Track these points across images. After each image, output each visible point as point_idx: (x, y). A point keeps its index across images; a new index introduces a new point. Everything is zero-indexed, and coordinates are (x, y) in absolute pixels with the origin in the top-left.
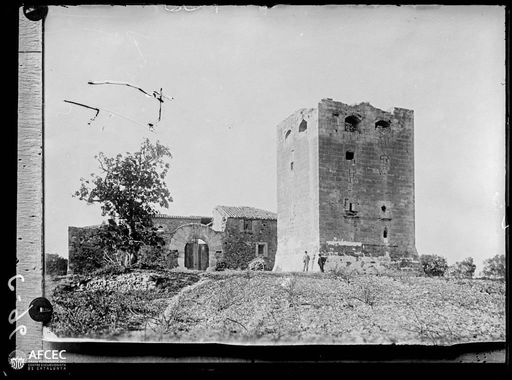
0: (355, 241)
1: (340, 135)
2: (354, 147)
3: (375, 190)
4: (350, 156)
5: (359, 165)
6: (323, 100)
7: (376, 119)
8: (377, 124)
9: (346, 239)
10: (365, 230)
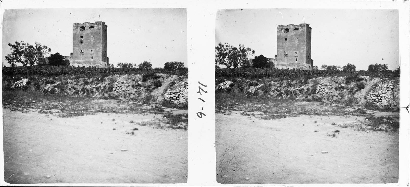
0: (287, 62)
1: (79, 32)
2: (287, 37)
3: (89, 46)
4: (286, 39)
5: (288, 42)
6: (278, 26)
7: (294, 28)
8: (90, 28)
9: (80, 60)
10: (290, 59)
